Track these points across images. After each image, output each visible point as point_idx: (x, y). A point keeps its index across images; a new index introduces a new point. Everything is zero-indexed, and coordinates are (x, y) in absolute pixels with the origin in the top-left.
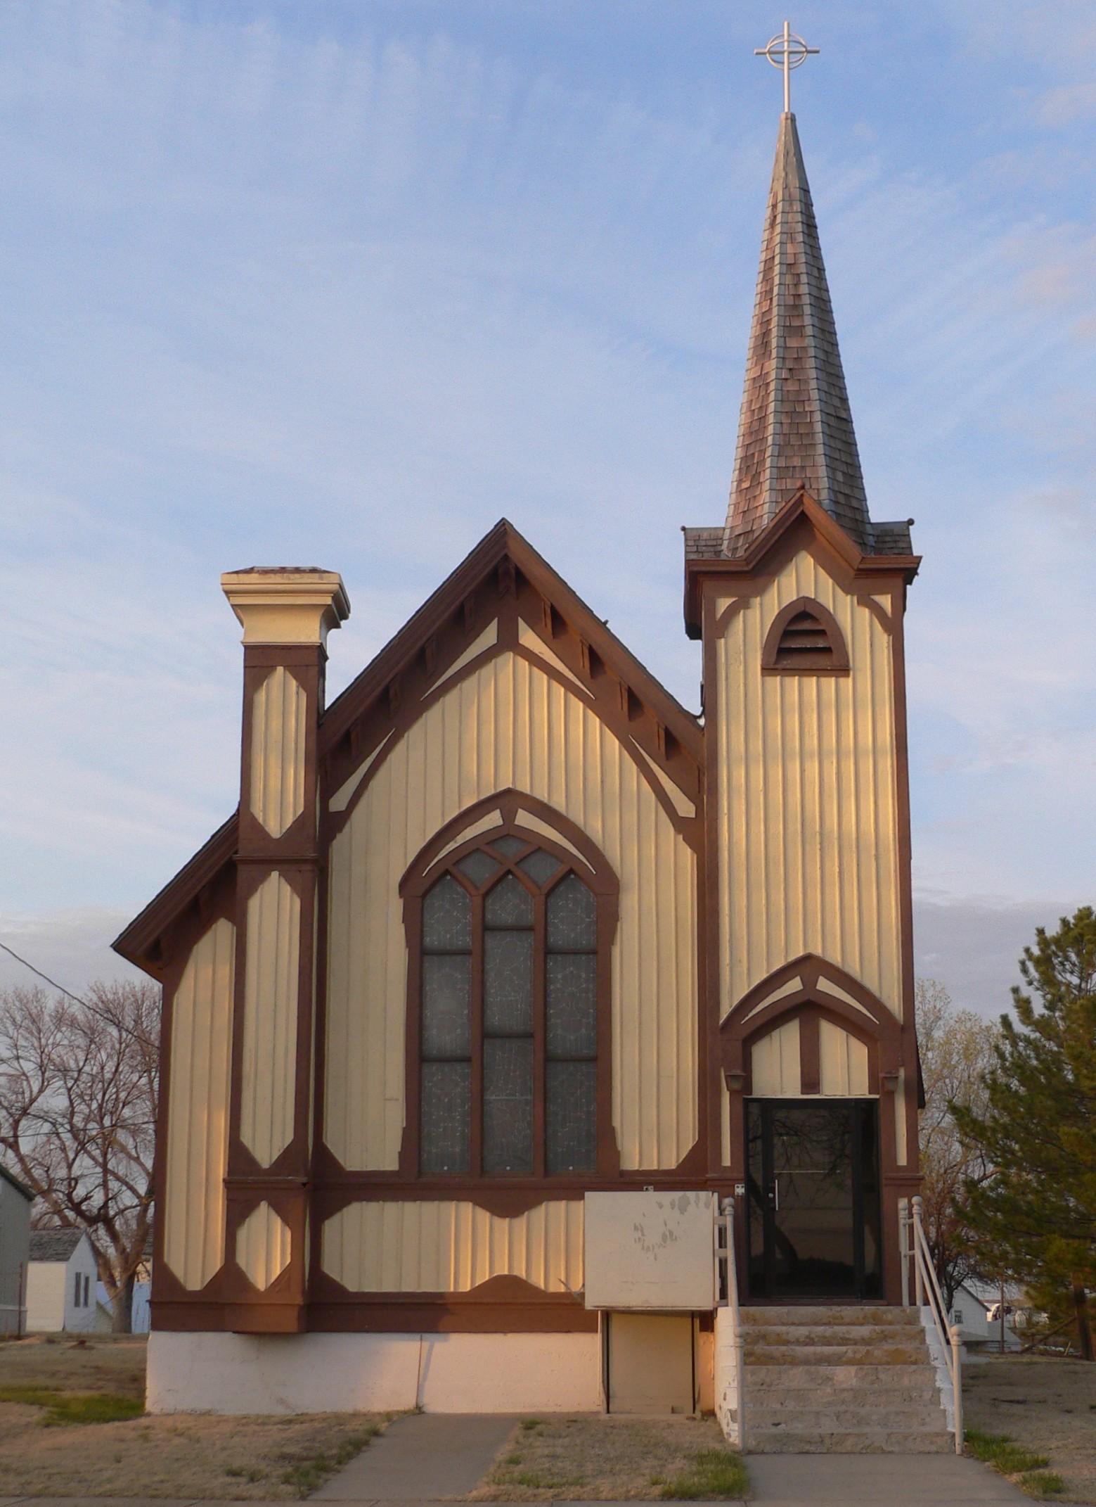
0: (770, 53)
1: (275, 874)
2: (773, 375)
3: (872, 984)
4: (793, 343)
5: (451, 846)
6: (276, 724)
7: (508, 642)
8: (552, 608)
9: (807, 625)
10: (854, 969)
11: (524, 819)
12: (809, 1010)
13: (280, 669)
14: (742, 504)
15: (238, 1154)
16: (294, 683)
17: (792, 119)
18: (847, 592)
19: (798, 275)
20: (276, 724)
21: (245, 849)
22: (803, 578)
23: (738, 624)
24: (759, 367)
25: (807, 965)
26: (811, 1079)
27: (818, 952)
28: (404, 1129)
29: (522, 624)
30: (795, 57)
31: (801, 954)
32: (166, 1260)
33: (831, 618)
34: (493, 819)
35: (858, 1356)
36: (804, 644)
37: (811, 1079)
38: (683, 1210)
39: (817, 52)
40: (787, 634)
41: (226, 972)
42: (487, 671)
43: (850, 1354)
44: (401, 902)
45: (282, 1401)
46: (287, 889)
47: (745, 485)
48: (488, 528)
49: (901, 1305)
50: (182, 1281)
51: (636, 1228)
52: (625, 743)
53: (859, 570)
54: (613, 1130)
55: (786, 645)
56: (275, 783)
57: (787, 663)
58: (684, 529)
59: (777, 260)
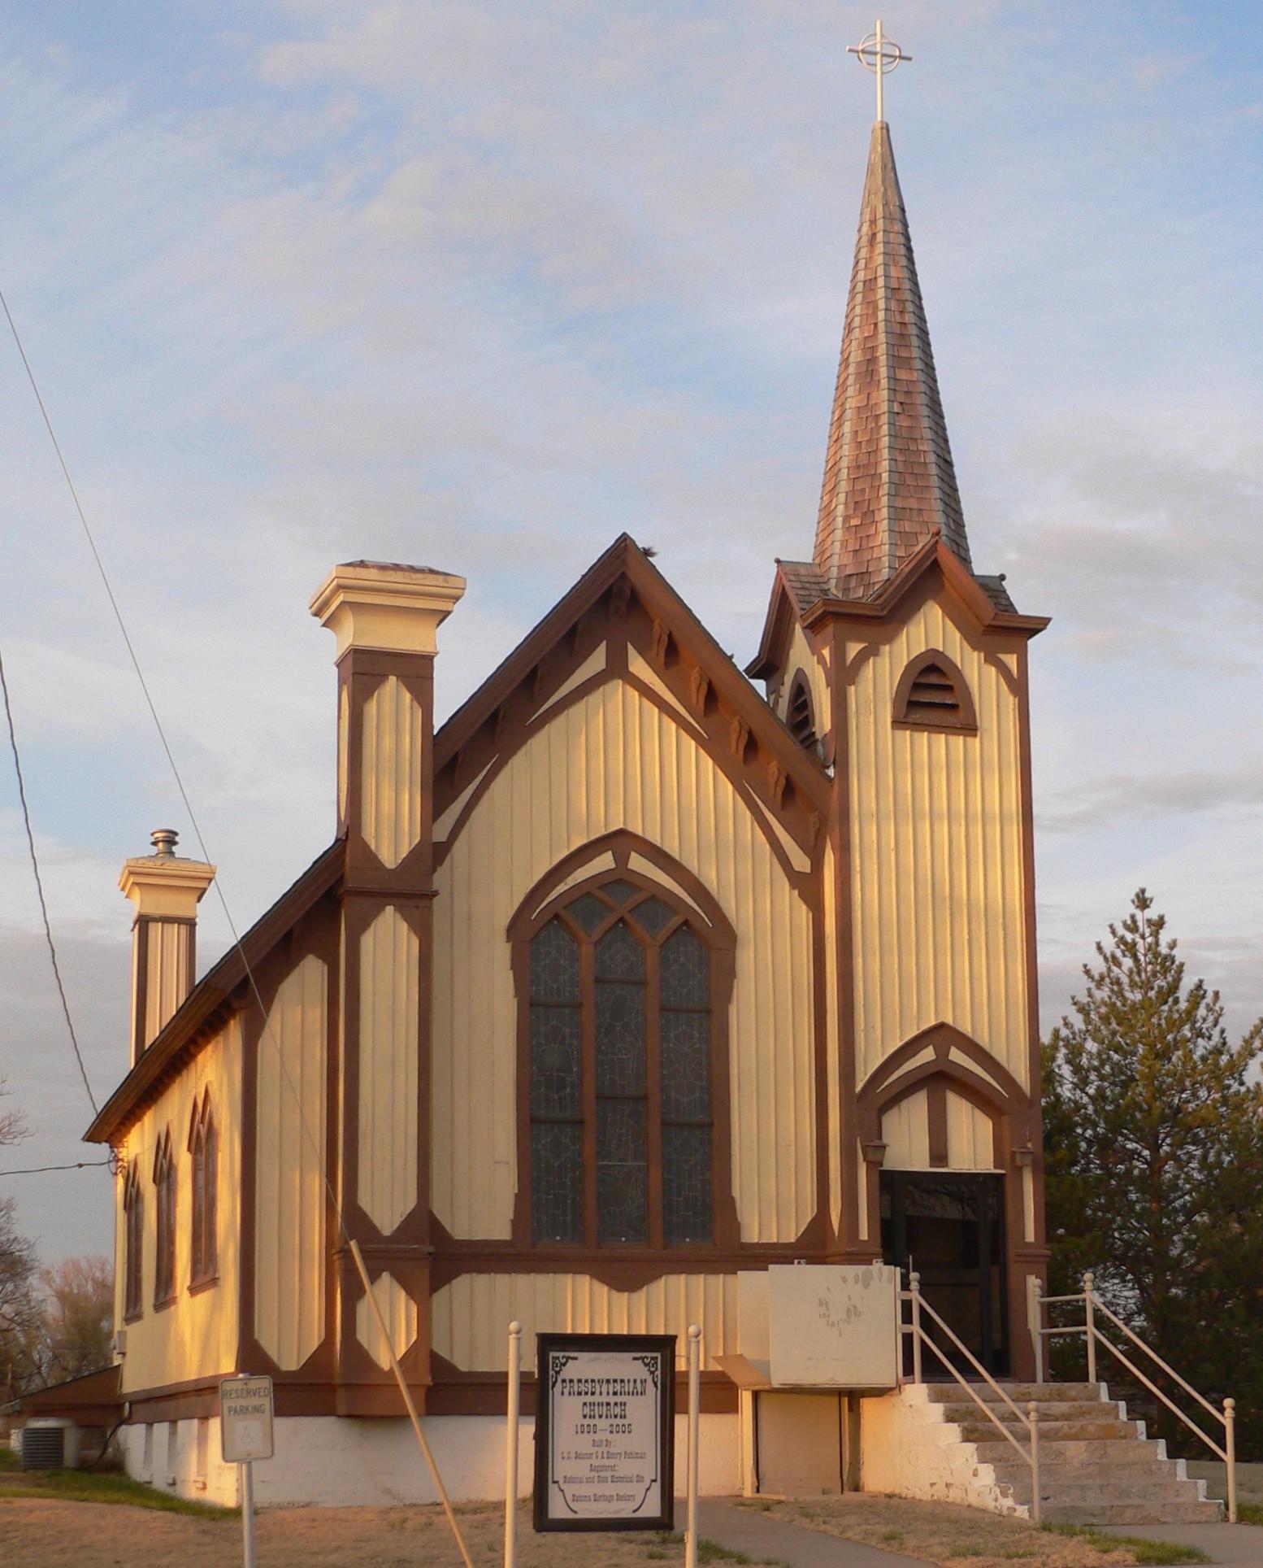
0: (863, 51)
1: (390, 909)
2: (884, 407)
3: (1000, 1055)
4: (903, 375)
5: (561, 888)
6: (388, 742)
7: (616, 669)
8: (670, 636)
9: (933, 679)
10: (984, 1041)
11: (638, 863)
12: (939, 1081)
13: (392, 679)
14: (851, 542)
15: (350, 1222)
16: (407, 696)
17: (886, 128)
18: (974, 648)
19: (904, 301)
20: (388, 742)
21: (351, 882)
22: (931, 630)
23: (868, 671)
24: (864, 396)
25: (941, 1034)
26: (939, 1154)
27: (949, 1020)
28: (516, 1195)
29: (631, 649)
30: (886, 60)
31: (933, 1023)
32: (256, 1336)
33: (958, 672)
34: (604, 862)
35: (1073, 1431)
36: (932, 698)
37: (939, 1154)
38: (866, 1285)
39: (910, 59)
40: (917, 687)
41: (317, 1016)
42: (595, 698)
43: (1066, 1429)
44: (508, 947)
45: (388, 1492)
46: (404, 927)
47: (855, 522)
48: (610, 542)
49: (1087, 1380)
50: (275, 1359)
51: (821, 1303)
52: (739, 788)
53: (990, 626)
54: (733, 1200)
55: (914, 699)
56: (387, 806)
57: (918, 716)
58: (778, 561)
59: (881, 282)
